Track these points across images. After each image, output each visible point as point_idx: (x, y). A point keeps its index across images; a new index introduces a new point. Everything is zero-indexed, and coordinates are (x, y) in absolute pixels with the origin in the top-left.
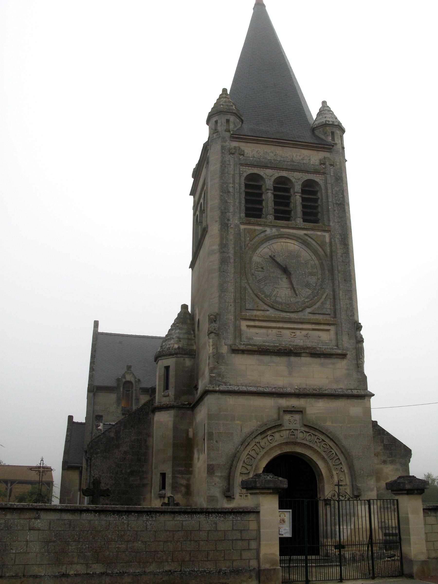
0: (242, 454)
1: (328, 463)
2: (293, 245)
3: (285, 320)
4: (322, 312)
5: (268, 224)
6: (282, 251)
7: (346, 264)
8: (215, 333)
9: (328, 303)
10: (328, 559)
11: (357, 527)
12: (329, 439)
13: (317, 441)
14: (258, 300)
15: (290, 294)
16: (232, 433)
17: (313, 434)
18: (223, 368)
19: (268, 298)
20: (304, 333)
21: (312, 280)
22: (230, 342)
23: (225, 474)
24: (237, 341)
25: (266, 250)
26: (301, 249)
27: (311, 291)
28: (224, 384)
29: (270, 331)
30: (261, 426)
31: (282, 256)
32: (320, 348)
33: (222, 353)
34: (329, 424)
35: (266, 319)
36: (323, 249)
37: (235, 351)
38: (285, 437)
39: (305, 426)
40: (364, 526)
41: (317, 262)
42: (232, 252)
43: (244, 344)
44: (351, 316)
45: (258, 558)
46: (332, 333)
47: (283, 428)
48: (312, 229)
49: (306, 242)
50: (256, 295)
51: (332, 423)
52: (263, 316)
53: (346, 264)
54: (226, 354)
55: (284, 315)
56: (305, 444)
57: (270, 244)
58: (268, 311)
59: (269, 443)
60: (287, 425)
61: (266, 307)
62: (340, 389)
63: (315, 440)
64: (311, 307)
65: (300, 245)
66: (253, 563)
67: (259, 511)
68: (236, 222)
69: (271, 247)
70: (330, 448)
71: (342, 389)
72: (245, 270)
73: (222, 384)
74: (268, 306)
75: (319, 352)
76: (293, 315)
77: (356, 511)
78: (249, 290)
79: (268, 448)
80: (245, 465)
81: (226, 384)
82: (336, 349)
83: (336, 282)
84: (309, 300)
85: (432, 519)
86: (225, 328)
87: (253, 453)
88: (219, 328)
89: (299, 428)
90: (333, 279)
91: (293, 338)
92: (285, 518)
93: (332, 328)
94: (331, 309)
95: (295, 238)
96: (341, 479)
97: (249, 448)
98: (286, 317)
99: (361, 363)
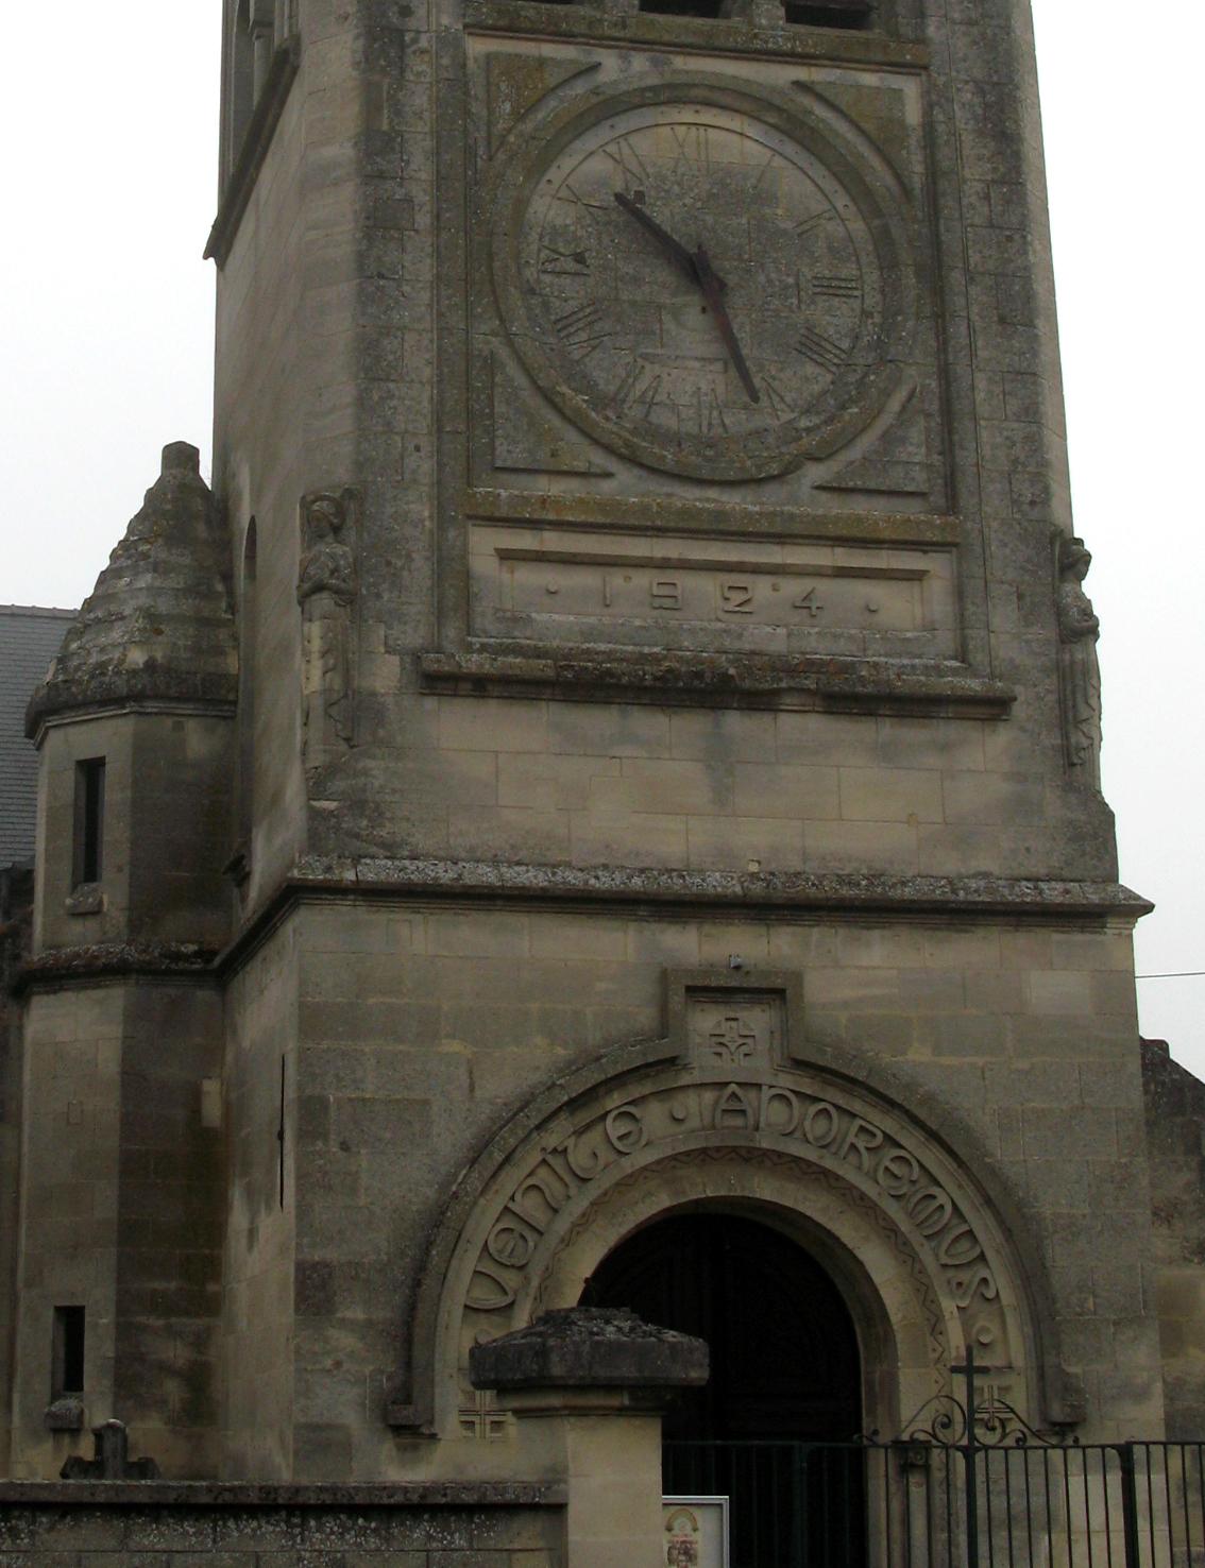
0: (477, 1210)
2: (736, 138)
3: (693, 525)
5: (608, 32)
6: (681, 170)
8: (337, 591)
9: (916, 434)
12: (920, 1135)
13: (861, 1145)
15: (721, 389)
16: (426, 1102)
17: (837, 1107)
18: (377, 770)
20: (793, 588)
22: (413, 635)
25: (599, 166)
26: (778, 162)
27: (829, 377)
28: (381, 852)
29: (617, 579)
30: (571, 1068)
31: (679, 197)
32: (876, 665)
33: (373, 694)
34: (918, 1054)
35: (600, 519)
37: (439, 683)
38: (694, 1123)
41: (858, 226)
43: (484, 648)
44: (1033, 503)
46: (938, 588)
47: (686, 1079)
48: (834, 59)
50: (549, 397)
52: (581, 501)
54: (390, 700)
56: (797, 1160)
58: (609, 475)
59: (612, 1156)
60: (704, 1063)
61: (600, 459)
63: (851, 1138)
65: (774, 139)
67: (558, 1500)
68: (445, 21)
69: (626, 150)
70: (924, 1181)
71: (986, 875)
72: (490, 268)
73: (373, 850)
74: (609, 449)
75: (870, 689)
76: (735, 501)
79: (606, 1181)
80: (488, 1267)
81: (391, 850)
82: (955, 672)
83: (958, 330)
84: (816, 420)
86: (389, 563)
87: (530, 1206)
89: (766, 1079)
91: (736, 618)
93: (936, 565)
94: (929, 467)
95: (746, 106)
97: (511, 1180)
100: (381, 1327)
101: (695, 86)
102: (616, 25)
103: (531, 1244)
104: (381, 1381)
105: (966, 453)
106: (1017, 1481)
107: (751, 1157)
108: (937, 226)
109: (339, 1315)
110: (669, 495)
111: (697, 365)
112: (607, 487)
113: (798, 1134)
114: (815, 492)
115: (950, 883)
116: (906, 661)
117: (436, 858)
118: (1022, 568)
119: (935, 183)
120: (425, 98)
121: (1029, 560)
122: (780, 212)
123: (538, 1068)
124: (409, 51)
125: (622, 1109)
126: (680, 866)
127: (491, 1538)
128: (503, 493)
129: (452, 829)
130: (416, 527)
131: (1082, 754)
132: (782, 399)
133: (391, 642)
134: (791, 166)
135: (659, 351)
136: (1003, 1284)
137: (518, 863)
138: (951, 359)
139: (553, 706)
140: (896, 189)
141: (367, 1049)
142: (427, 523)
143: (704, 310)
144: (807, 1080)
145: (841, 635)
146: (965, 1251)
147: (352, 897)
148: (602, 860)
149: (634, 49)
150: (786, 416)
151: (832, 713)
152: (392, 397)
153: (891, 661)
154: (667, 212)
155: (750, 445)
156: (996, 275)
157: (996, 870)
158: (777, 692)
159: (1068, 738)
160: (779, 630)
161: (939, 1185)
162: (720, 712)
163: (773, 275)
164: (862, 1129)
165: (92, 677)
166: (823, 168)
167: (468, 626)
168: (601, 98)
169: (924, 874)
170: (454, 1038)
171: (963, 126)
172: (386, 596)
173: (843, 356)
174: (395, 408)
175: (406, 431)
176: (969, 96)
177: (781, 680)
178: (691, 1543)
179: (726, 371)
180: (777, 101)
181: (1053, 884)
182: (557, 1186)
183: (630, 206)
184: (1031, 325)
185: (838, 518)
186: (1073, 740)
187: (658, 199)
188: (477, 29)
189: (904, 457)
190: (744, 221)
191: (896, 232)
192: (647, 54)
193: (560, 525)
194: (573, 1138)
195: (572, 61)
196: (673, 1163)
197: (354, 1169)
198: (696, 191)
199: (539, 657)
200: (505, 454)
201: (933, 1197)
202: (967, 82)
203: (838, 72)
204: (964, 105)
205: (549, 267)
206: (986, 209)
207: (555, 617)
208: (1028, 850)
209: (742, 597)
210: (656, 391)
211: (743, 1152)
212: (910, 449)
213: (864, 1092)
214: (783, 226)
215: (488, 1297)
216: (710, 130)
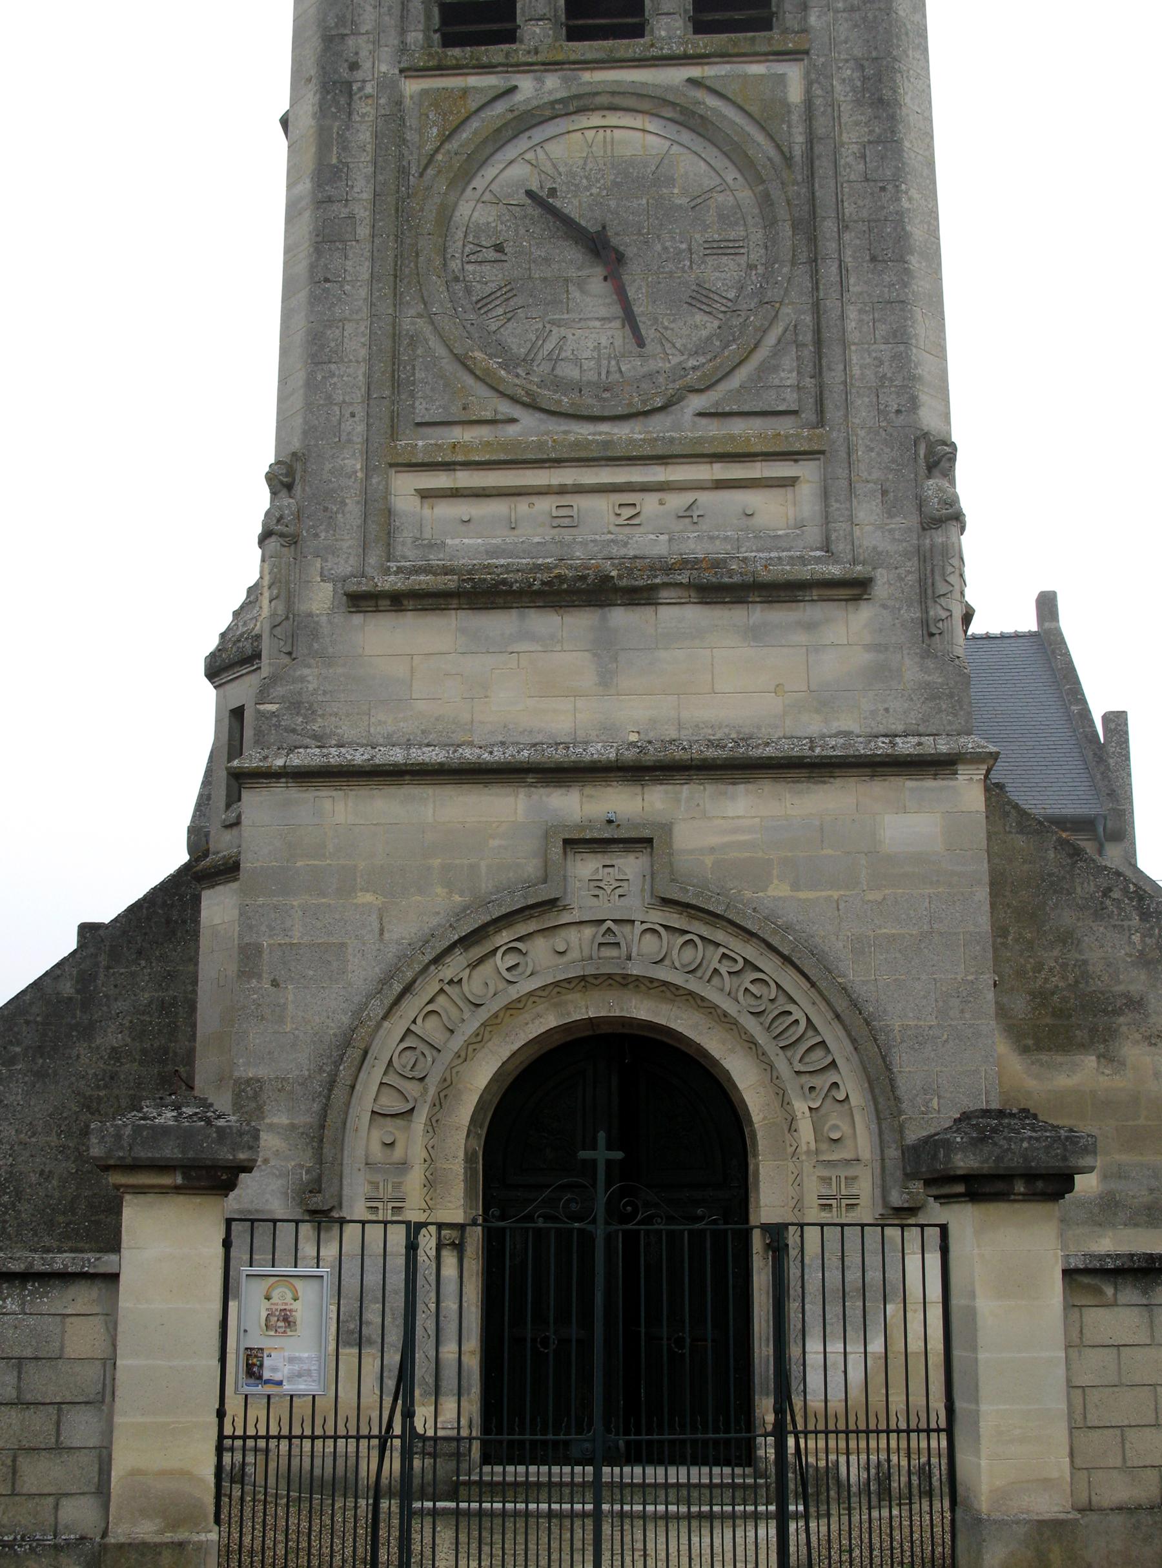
0: (382, 1032)
1: (772, 1066)
2: (639, 134)
3: (583, 454)
4: (759, 406)
5: (523, 59)
6: (590, 166)
7: (883, 189)
8: (282, 535)
9: (788, 361)
10: (756, 1486)
11: (897, 1346)
12: (778, 961)
13: (723, 970)
14: (470, 381)
15: (618, 342)
16: (343, 945)
17: (702, 938)
18: (311, 676)
19: (520, 371)
20: (677, 501)
21: (723, 275)
22: (344, 565)
23: (305, 1119)
24: (372, 560)
25: (519, 171)
26: (675, 149)
27: (716, 323)
28: (313, 743)
29: (522, 506)
30: (461, 913)
31: (587, 188)
32: (745, 560)
33: (310, 615)
34: (778, 890)
35: (502, 457)
36: (771, 138)
37: (362, 601)
38: (574, 954)
39: (666, 902)
40: (915, 1345)
41: (745, 195)
42: (365, 196)
43: (400, 570)
44: (898, 412)
45: (102, 1490)
46: (807, 491)
47: (566, 918)
48: (724, 56)
49: (693, 113)
50: (463, 361)
51: (795, 886)
52: (488, 444)
53: (883, 189)
54: (324, 619)
55: (584, 431)
56: (665, 984)
57: (535, 141)
58: (513, 421)
59: (502, 985)
60: (582, 904)
61: (506, 408)
62: (836, 735)
63: (715, 964)
64: (708, 388)
65: (672, 130)
66: (79, 1515)
67: (114, 1270)
68: (384, 68)
69: (541, 155)
70: (782, 999)
71: (847, 734)
72: (416, 263)
73: (308, 741)
74: (514, 400)
75: (736, 579)
76: (622, 432)
77: (893, 1275)
78: (434, 342)
79: (495, 1006)
80: (391, 1079)
81: (320, 740)
82: (818, 560)
83: (830, 271)
84: (702, 360)
85: (1118, 1318)
86: (326, 509)
87: (430, 1029)
88: (298, 516)
89: (637, 916)
90: (815, 260)
91: (627, 530)
92: (296, 1305)
93: (806, 471)
94: (799, 388)
95: (646, 105)
96: (835, 1136)
97: (412, 1006)
98: (593, 441)
99: (944, 614)
100: (301, 1130)
101: (597, 94)
102: (529, 52)
103: (429, 1059)
104: (301, 1174)
105: (833, 374)
106: (853, 1259)
107: (626, 982)
108: (813, 185)
109: (267, 1121)
110: (566, 432)
111: (597, 324)
112: (512, 430)
113: (667, 962)
114: (697, 419)
115: (811, 742)
116: (773, 555)
117: (358, 744)
118: (887, 468)
119: (812, 148)
120: (368, 134)
121: (893, 461)
122: (676, 191)
123: (438, 913)
124: (356, 98)
125: (510, 945)
126: (567, 740)
127: (46, 1304)
128: (420, 443)
129: (373, 720)
130: (350, 477)
131: (940, 625)
132: (674, 346)
133: (326, 573)
134: (685, 151)
135: (566, 316)
136: (852, 1085)
137: (428, 745)
138: (821, 295)
139: (461, 614)
140: (777, 159)
141: (295, 903)
142: (359, 474)
143: (605, 279)
144: (675, 915)
145: (718, 537)
146: (818, 1059)
147: (283, 780)
148: (500, 738)
149: (546, 71)
150: (675, 360)
151: (707, 603)
152: (333, 375)
153: (761, 555)
154: (576, 202)
155: (644, 386)
156: (869, 221)
157: (856, 729)
158: (654, 588)
159: (927, 612)
160: (661, 537)
161: (795, 1003)
162: (607, 609)
163: (668, 244)
164: (724, 956)
165: (234, 644)
166: (715, 150)
167: (389, 554)
168: (516, 113)
169: (788, 734)
170: (368, 891)
171: (842, 98)
172: (323, 535)
173: (729, 304)
174: (335, 384)
175: (344, 402)
176: (849, 72)
177: (656, 577)
178: (290, 1311)
179: (624, 327)
180: (670, 98)
181: (910, 739)
182: (454, 1013)
183: (542, 203)
184: (902, 260)
185: (714, 438)
186: (932, 613)
187: (568, 192)
188: (410, 72)
189: (777, 382)
190: (644, 201)
191: (776, 194)
192: (559, 73)
193: (467, 465)
194: (468, 970)
195: (491, 87)
196: (558, 989)
197: (282, 1001)
198: (602, 181)
199: (446, 574)
200: (423, 411)
201: (790, 1013)
202: (847, 61)
203: (728, 67)
204: (844, 80)
205: (473, 258)
206: (862, 166)
207: (466, 541)
208: (887, 710)
209: (630, 512)
210: (561, 349)
211: (618, 979)
212: (782, 375)
213: (725, 924)
214: (678, 202)
215: (392, 1103)
216: (615, 130)
